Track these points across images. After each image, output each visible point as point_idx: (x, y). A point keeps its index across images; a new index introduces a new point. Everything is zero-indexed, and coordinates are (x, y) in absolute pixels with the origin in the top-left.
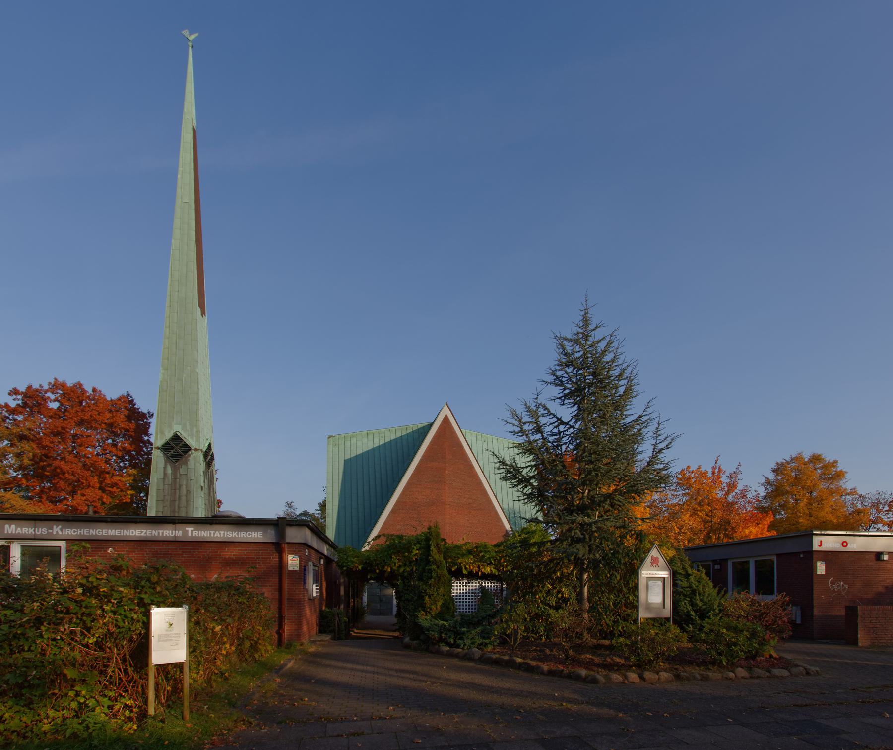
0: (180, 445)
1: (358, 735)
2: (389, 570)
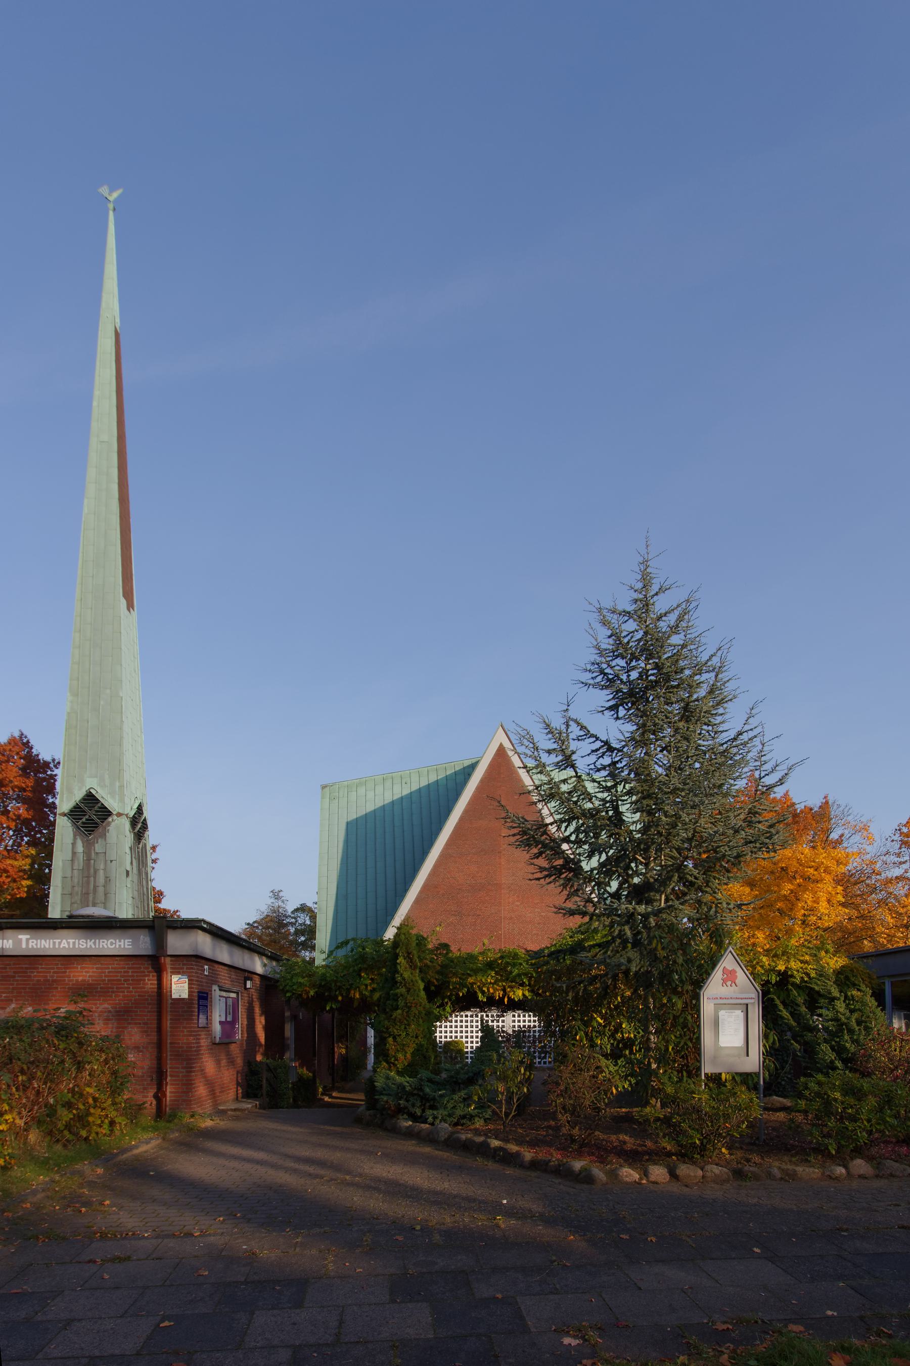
0: (96, 808)
1: (119, 1262)
2: (358, 996)
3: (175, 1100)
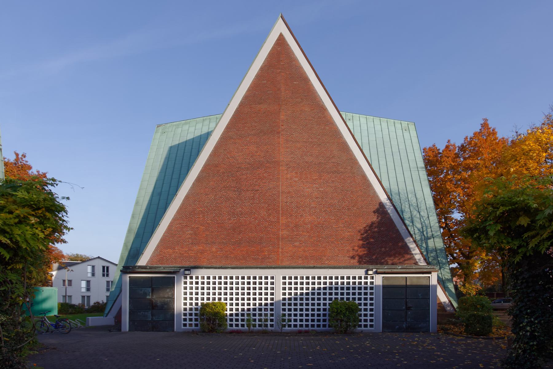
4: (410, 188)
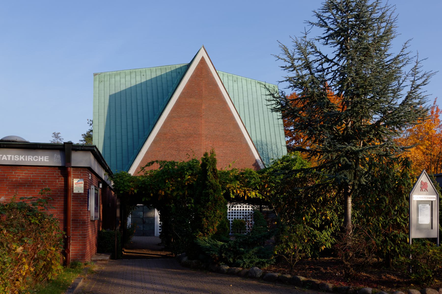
3: (75, 255)
4: (273, 140)
